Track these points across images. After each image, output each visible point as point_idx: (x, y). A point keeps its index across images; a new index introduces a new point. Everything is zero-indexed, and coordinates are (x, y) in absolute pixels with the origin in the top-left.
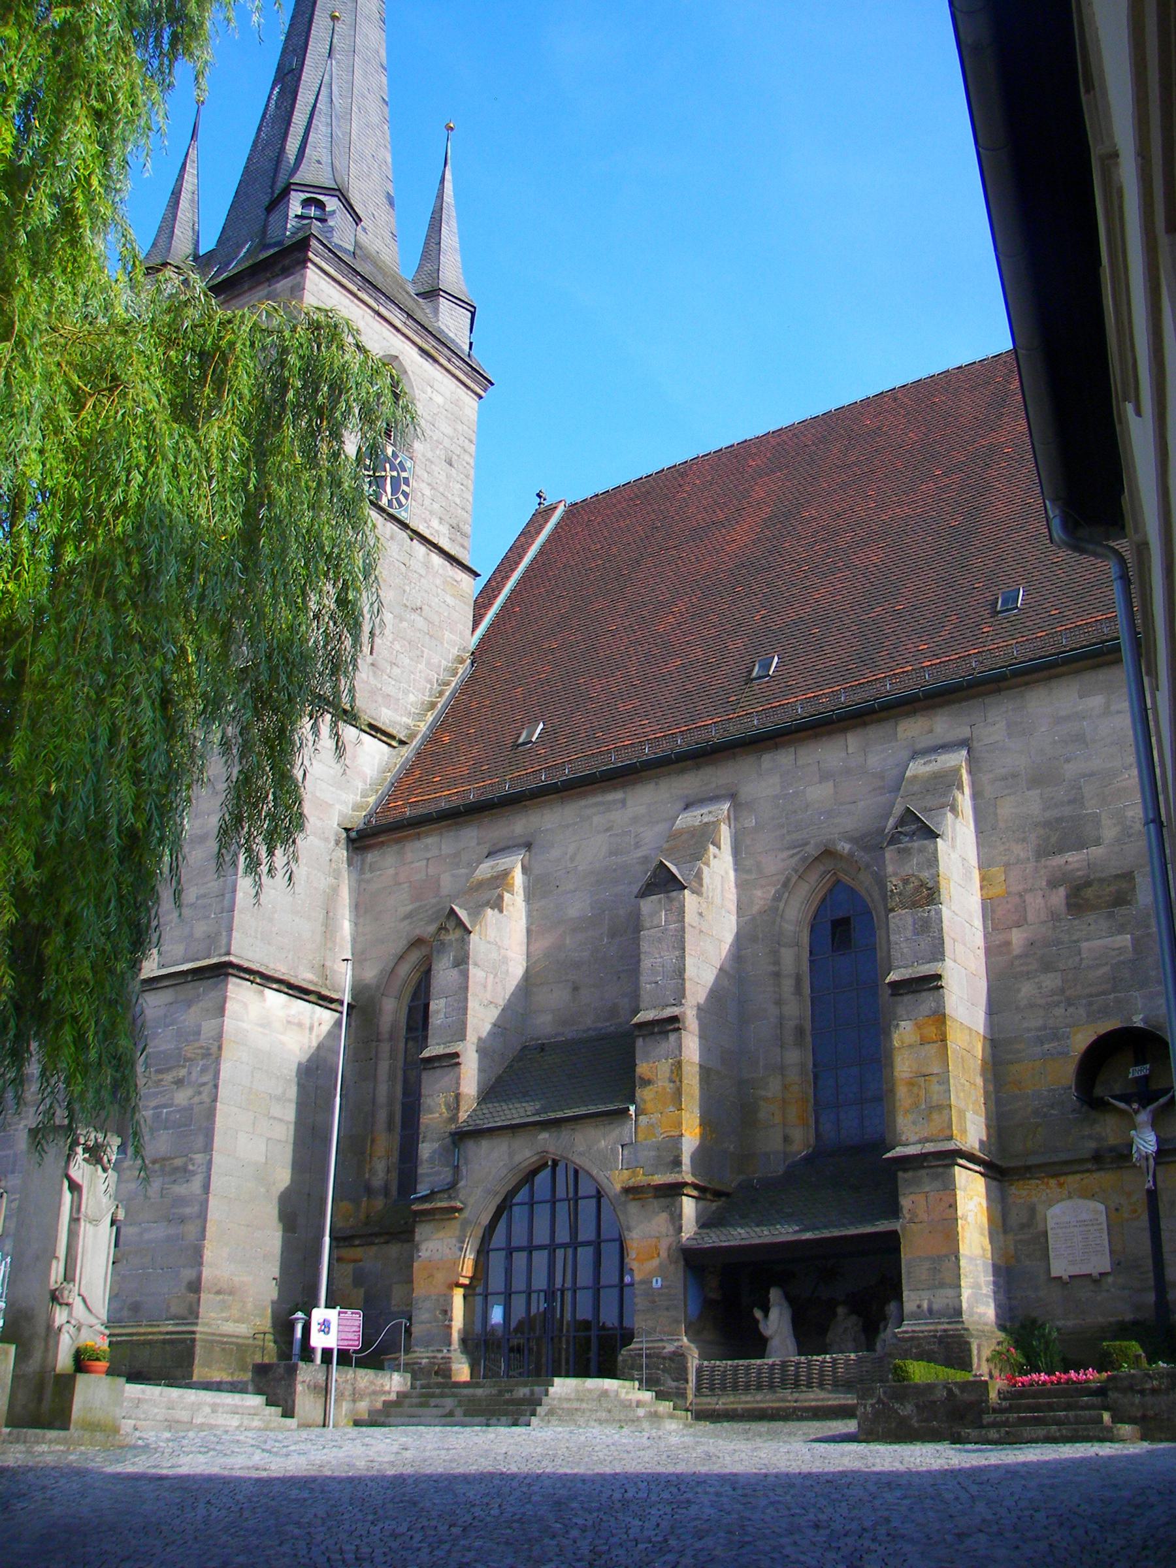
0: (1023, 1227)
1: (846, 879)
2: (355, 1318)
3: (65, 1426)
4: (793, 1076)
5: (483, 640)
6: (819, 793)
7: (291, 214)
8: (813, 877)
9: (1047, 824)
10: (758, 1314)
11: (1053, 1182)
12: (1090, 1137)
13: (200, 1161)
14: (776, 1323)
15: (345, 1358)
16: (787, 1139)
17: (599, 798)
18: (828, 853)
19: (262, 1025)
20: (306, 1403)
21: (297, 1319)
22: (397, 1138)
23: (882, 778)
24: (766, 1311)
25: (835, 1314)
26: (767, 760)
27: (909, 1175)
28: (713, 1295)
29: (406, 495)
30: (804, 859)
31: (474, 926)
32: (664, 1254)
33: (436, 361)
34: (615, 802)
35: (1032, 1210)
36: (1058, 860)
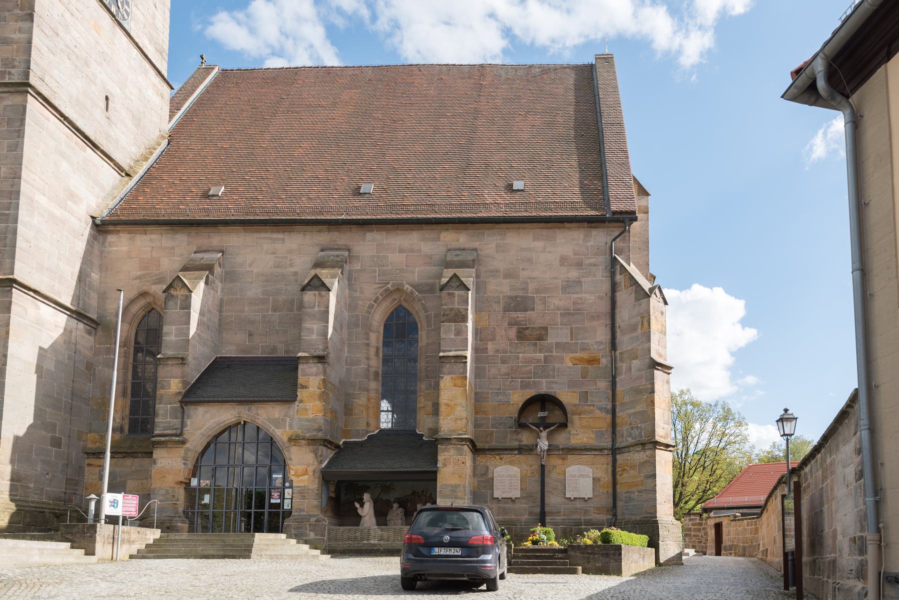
0: (482, 475)
1: (406, 305)
6: (395, 259)
8: (390, 300)
9: (510, 297)
10: (357, 505)
11: (498, 457)
12: (516, 440)
14: (367, 510)
16: (368, 424)
17: (268, 235)
18: (399, 289)
20: (102, 547)
21: (91, 499)
23: (431, 258)
24: (362, 506)
26: (369, 236)
27: (443, 447)
28: (333, 495)
30: (387, 290)
32: (311, 473)
34: (278, 239)
35: (487, 468)
36: (514, 315)
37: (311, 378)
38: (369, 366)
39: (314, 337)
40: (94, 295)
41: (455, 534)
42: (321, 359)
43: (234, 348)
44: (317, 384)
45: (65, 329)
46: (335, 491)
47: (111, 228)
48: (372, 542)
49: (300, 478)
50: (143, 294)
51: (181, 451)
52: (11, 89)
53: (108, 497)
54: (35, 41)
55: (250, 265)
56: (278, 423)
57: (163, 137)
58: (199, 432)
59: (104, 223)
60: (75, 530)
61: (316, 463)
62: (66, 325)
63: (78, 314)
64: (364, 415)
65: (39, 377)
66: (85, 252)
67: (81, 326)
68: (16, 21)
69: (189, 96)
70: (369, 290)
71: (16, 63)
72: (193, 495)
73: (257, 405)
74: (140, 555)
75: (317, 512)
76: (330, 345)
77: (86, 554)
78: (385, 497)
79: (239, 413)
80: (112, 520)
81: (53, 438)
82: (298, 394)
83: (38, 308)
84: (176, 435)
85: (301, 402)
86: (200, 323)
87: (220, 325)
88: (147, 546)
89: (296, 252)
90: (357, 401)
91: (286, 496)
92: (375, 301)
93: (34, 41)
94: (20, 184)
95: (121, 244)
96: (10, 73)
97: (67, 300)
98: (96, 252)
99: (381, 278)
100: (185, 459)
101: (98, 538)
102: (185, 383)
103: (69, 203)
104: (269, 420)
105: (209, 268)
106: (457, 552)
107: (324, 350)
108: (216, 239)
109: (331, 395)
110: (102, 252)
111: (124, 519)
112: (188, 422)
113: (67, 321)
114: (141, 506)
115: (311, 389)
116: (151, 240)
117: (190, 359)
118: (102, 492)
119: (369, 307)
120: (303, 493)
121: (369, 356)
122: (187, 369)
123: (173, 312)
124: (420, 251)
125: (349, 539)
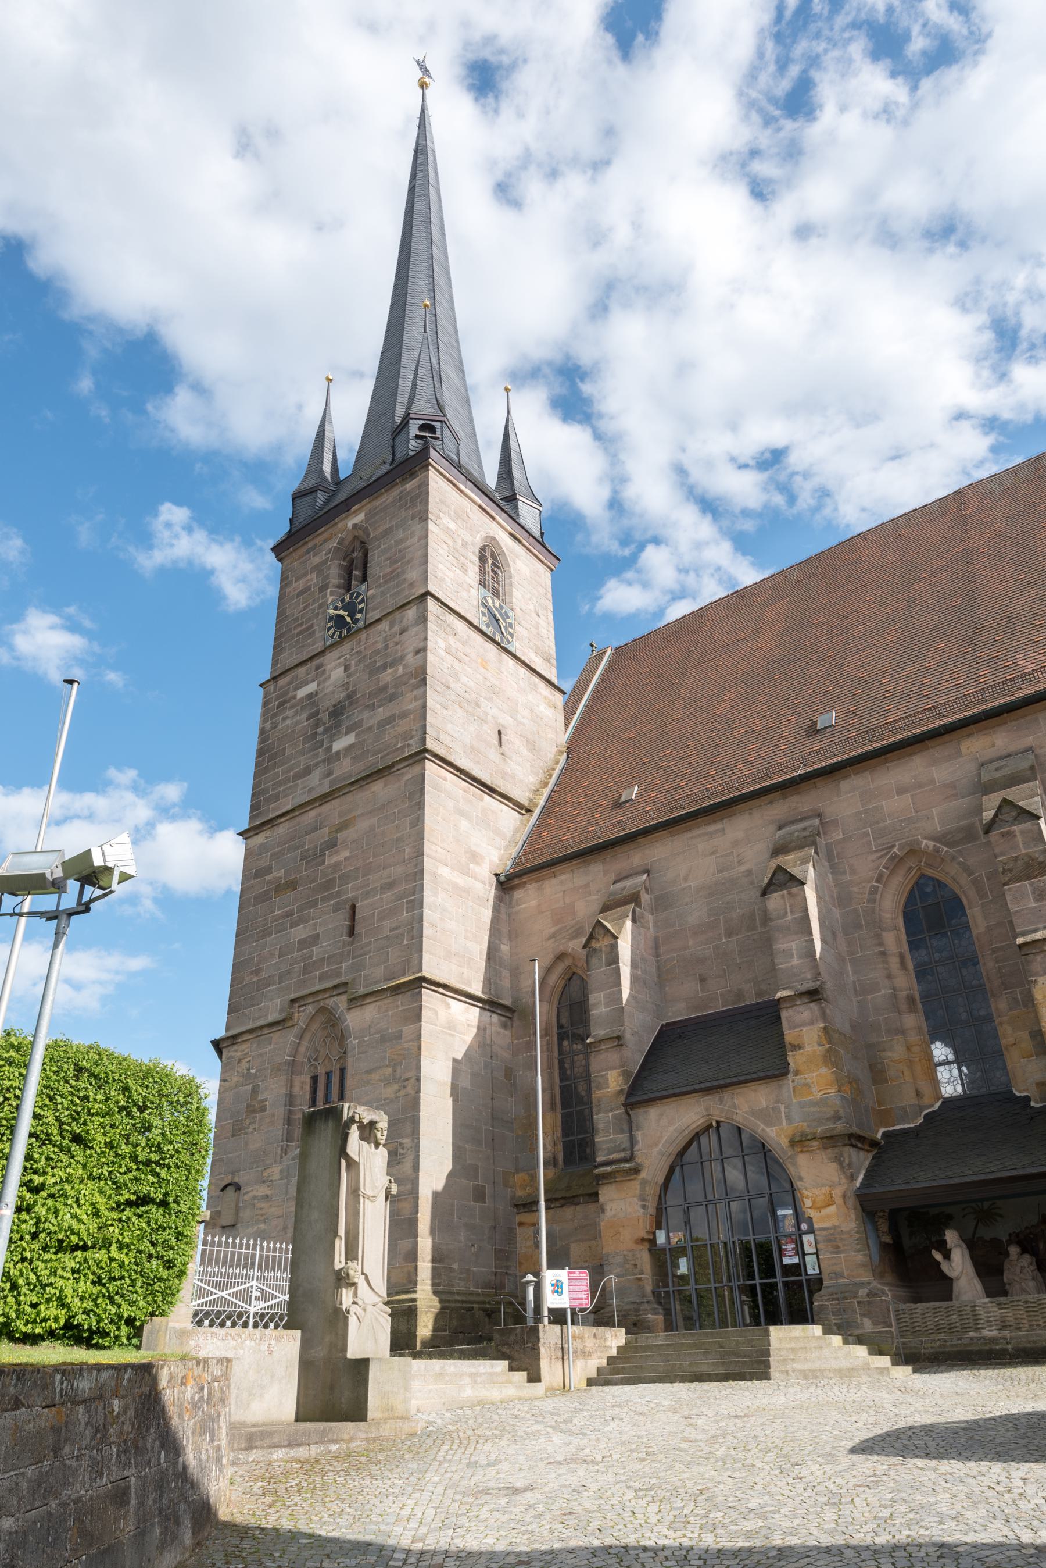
1: (930, 872)
2: (583, 1278)
3: (364, 1419)
5: (578, 730)
6: (895, 806)
7: (412, 435)
8: (902, 872)
10: (938, 1256)
13: (409, 1145)
15: (576, 1316)
16: (918, 1093)
18: (913, 851)
19: (449, 1028)
21: (529, 1282)
22: (559, 1115)
23: (954, 787)
25: (1008, 1254)
26: (845, 785)
28: (887, 1239)
29: (512, 635)
30: (892, 858)
32: (839, 1201)
33: (520, 542)
34: (716, 831)
37: (804, 1031)
38: (894, 989)
39: (795, 961)
40: (506, 973)
42: (813, 995)
43: (682, 1005)
45: (478, 1027)
47: (516, 881)
48: (986, 1333)
49: (824, 1212)
50: (561, 957)
52: (411, 761)
53: (550, 1276)
55: (686, 879)
56: (769, 1116)
57: (561, 752)
59: (510, 877)
60: (512, 1338)
61: (844, 1181)
62: (480, 1021)
63: (489, 1004)
67: (495, 1018)
69: (583, 694)
70: (864, 866)
71: (414, 733)
73: (730, 1091)
75: (866, 1276)
76: (822, 969)
78: (987, 1233)
79: (707, 1109)
80: (558, 1317)
82: (790, 1060)
83: (448, 1006)
84: (626, 1160)
85: (797, 1073)
86: (634, 979)
87: (659, 977)
88: (609, 1359)
89: (742, 844)
90: (889, 1054)
91: (808, 1249)
92: (878, 881)
93: (428, 704)
95: (529, 898)
96: (409, 745)
97: (476, 989)
98: (504, 916)
101: (542, 1350)
102: (626, 1074)
103: (472, 866)
104: (753, 1113)
105: (634, 899)
108: (636, 857)
110: (509, 915)
111: (574, 1312)
112: (639, 1136)
113: (480, 1015)
115: (808, 1049)
116: (562, 883)
117: (628, 1036)
120: (833, 1239)
121: (891, 971)
122: (627, 1052)
123: (598, 972)
124: (933, 781)
125: (939, 1329)
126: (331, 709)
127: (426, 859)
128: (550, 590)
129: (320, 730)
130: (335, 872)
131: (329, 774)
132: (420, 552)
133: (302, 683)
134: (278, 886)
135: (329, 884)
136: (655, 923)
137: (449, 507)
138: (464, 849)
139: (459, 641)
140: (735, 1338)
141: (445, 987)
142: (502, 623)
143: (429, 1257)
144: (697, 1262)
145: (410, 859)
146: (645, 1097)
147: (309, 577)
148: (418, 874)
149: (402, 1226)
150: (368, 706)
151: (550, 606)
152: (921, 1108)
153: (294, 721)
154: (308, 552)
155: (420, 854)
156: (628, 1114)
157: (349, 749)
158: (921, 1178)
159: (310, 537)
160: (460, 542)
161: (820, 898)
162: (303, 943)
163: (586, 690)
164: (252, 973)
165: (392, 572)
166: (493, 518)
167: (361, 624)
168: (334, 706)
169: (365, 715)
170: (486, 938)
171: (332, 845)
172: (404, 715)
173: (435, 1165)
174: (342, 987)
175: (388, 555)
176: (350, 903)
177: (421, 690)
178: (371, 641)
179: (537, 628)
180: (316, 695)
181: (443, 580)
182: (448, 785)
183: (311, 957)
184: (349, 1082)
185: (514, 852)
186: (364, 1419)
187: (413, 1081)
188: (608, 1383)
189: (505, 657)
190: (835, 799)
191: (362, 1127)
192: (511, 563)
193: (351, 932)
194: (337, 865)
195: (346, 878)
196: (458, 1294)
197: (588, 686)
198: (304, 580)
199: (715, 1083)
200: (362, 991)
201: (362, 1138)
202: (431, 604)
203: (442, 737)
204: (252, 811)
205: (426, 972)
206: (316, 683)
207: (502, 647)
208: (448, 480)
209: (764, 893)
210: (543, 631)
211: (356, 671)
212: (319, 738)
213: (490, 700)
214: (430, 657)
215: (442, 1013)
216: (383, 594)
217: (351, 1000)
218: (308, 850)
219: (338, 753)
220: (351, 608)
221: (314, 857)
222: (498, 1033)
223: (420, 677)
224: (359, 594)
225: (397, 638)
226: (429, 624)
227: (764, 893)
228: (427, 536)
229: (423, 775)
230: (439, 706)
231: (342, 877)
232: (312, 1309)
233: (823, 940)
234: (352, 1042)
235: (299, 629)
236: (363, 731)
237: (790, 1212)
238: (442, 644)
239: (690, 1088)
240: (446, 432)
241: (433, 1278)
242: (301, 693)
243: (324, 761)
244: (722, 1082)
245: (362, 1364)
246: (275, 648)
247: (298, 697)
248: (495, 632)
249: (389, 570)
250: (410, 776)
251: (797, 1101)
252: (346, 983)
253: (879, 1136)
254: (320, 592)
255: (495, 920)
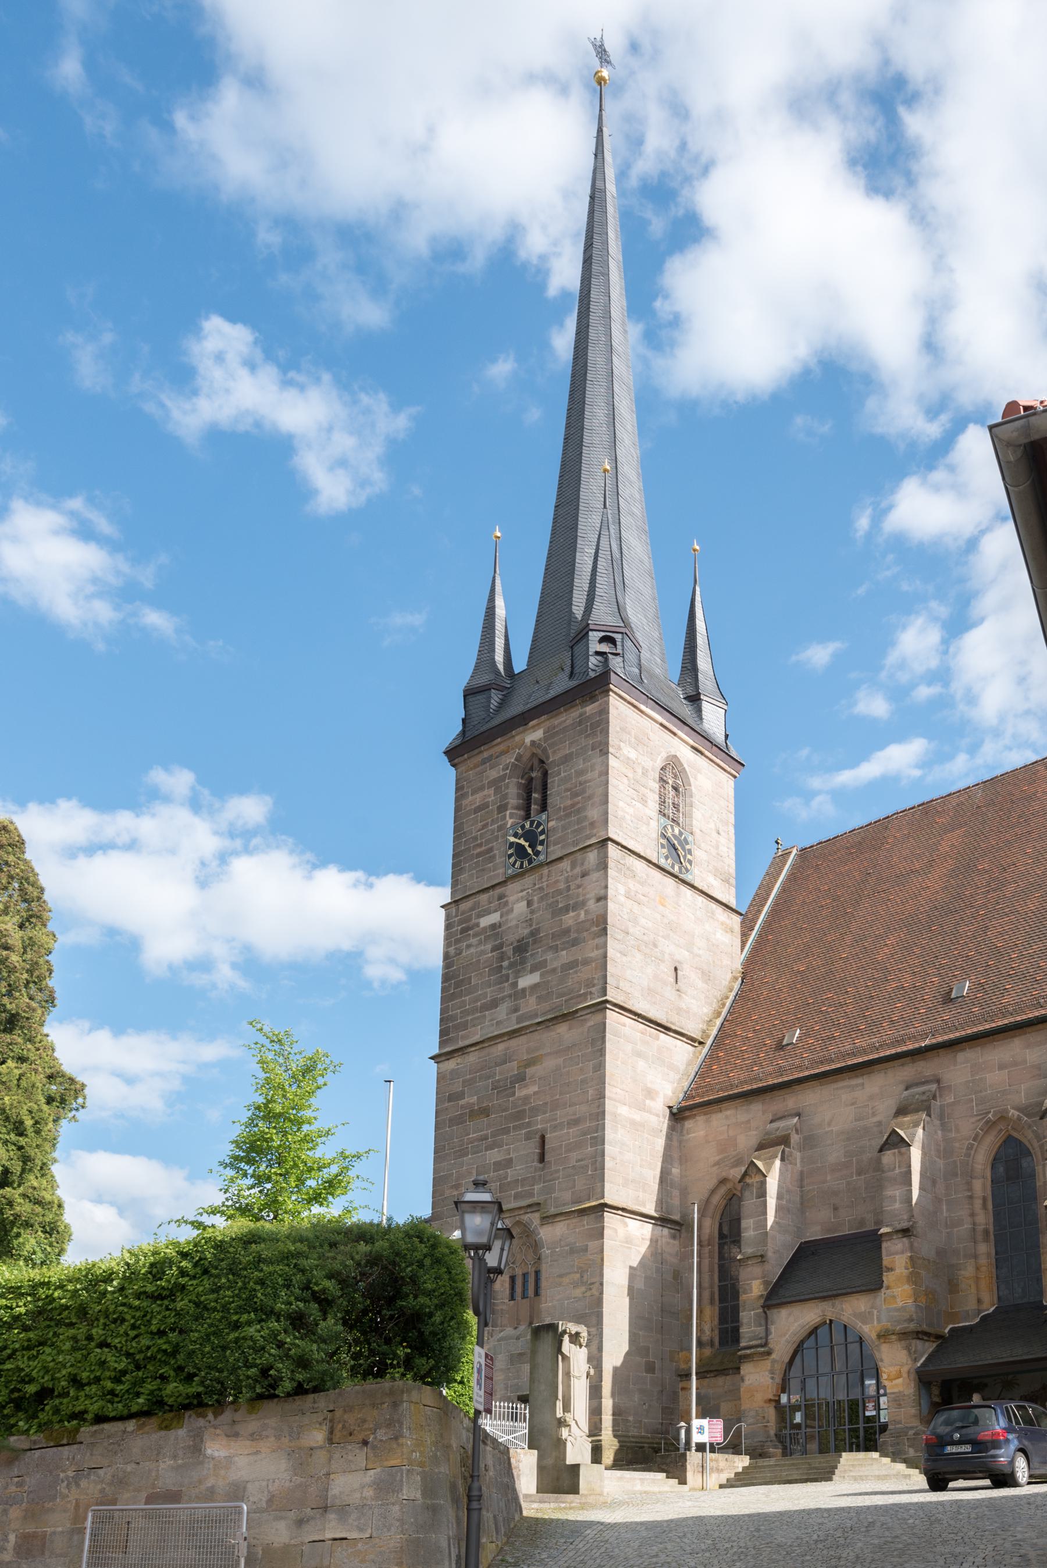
1: (1015, 1134)
2: (719, 1424)
3: (578, 1493)
4: (983, 1261)
6: (995, 1078)
7: (591, 651)
8: (994, 1133)
16: (979, 1301)
18: (1003, 1118)
19: (627, 1242)
22: (717, 1308)
23: (1040, 1069)
26: (961, 1056)
30: (987, 1122)
31: (768, 1171)
32: (905, 1375)
33: (702, 753)
34: (857, 1085)
37: (896, 1258)
38: (974, 1224)
39: (897, 1205)
40: (676, 1193)
41: (964, 1431)
42: (906, 1232)
43: (818, 1228)
44: (904, 1264)
45: (651, 1240)
46: (941, 1394)
47: (687, 1113)
49: (895, 1382)
50: (723, 1181)
51: (767, 1364)
52: (593, 1010)
53: (696, 1423)
54: (611, 953)
55: (829, 1125)
56: (865, 1318)
57: (736, 978)
58: (784, 1339)
59: (681, 1110)
60: (669, 1460)
61: (910, 1362)
62: (652, 1235)
63: (661, 1221)
64: (973, 1290)
65: (631, 1300)
66: (665, 1149)
67: (666, 1231)
68: (593, 939)
69: (763, 905)
70: (966, 1126)
71: (596, 981)
72: (783, 1413)
73: (840, 1299)
74: (729, 1484)
75: (916, 1423)
76: (916, 1212)
77: (680, 1483)
79: (823, 1311)
80: (701, 1447)
81: (648, 1363)
82: (884, 1279)
83: (626, 1225)
84: (761, 1346)
85: (888, 1288)
86: (779, 1209)
87: (802, 1204)
88: (736, 1474)
89: (877, 1095)
90: (963, 1272)
91: (882, 1406)
92: (974, 1140)
93: (609, 955)
94: (604, 1104)
95: (697, 1128)
96: (591, 993)
97: (650, 1209)
98: (675, 1143)
99: (980, 1107)
100: (772, 1372)
101: (688, 1467)
102: (766, 1283)
103: (647, 1102)
104: (855, 1315)
105: (784, 1140)
106: (968, 1448)
107: (909, 1220)
108: (790, 1101)
109: (923, 1272)
110: (680, 1142)
111: (711, 1445)
112: (773, 1328)
113: (653, 1230)
114: (726, 1430)
115: (898, 1271)
116: (727, 1117)
117: (770, 1254)
118: (691, 1419)
119: (968, 1149)
120: (897, 1401)
121: (974, 1212)
122: (767, 1267)
123: (749, 1203)
124: (1025, 1061)
126: (515, 944)
127: (607, 1101)
128: (732, 801)
129: (505, 964)
130: (525, 1104)
131: (516, 1010)
132: (600, 791)
133: (485, 910)
134: (472, 1111)
135: (519, 1115)
136: (802, 1159)
137: (629, 734)
138: (642, 1081)
139: (639, 882)
140: (819, 1461)
141: (623, 1210)
142: (681, 852)
143: (611, 1412)
144: (807, 1417)
145: (593, 1100)
146: (779, 1301)
147: (486, 792)
148: (601, 1115)
149: (595, 1391)
150: (551, 947)
151: (732, 819)
152: (979, 1311)
153: (479, 950)
154: (484, 762)
155: (601, 1096)
156: (765, 1313)
157: (534, 987)
158: (962, 1361)
159: (486, 747)
160: (640, 771)
161: (924, 1154)
162: (498, 1166)
163: (766, 900)
164: (452, 1187)
165: (573, 805)
166: (675, 734)
167: (542, 857)
168: (518, 941)
169: (549, 956)
170: (659, 1164)
171: (521, 1078)
172: (586, 962)
173: (616, 1346)
174: (535, 1207)
175: (568, 785)
176: (539, 1134)
177: (602, 939)
178: (553, 879)
179: (717, 848)
180: (500, 926)
181: (623, 818)
182: (627, 1030)
183: (506, 1178)
184: (544, 1284)
185: (686, 1084)
186: (578, 1493)
187: (597, 1284)
188: (732, 1486)
189: (684, 889)
190: (952, 1068)
191: (571, 1336)
192: (692, 780)
193: (542, 1158)
194: (526, 1099)
195: (535, 1111)
196: (633, 1437)
197: (769, 895)
198: (481, 794)
199: (830, 1293)
200: (553, 1211)
201: (571, 1342)
202: (612, 850)
203: (621, 984)
204: (441, 1036)
205: (608, 1199)
206: (499, 913)
207: (680, 880)
208: (629, 703)
209: (881, 1150)
210: (723, 850)
211: (539, 908)
212: (504, 972)
213: (666, 937)
214: (611, 906)
215: (621, 1232)
216: (564, 828)
217: (543, 1218)
218: (498, 1081)
219: (524, 990)
220: (531, 836)
221: (505, 1088)
222: (668, 1243)
223: (601, 926)
224: (539, 824)
225: (579, 881)
226: (610, 872)
227: (881, 1150)
228: (607, 773)
229: (604, 1024)
230: (619, 955)
231: (532, 1109)
232: (546, 1439)
233: (922, 1188)
234: (546, 1252)
235: (479, 850)
236: (547, 972)
237: (874, 1382)
238: (622, 890)
239: (812, 1296)
240: (628, 643)
241: (614, 1426)
242: (485, 922)
243: (510, 996)
244: (835, 1292)
245: (576, 1468)
246: (454, 866)
247: (482, 925)
248: (674, 859)
249: (569, 802)
250: (592, 1023)
251: (883, 1310)
252: (539, 1204)
253: (947, 1331)
254: (499, 813)
255: (668, 1148)
